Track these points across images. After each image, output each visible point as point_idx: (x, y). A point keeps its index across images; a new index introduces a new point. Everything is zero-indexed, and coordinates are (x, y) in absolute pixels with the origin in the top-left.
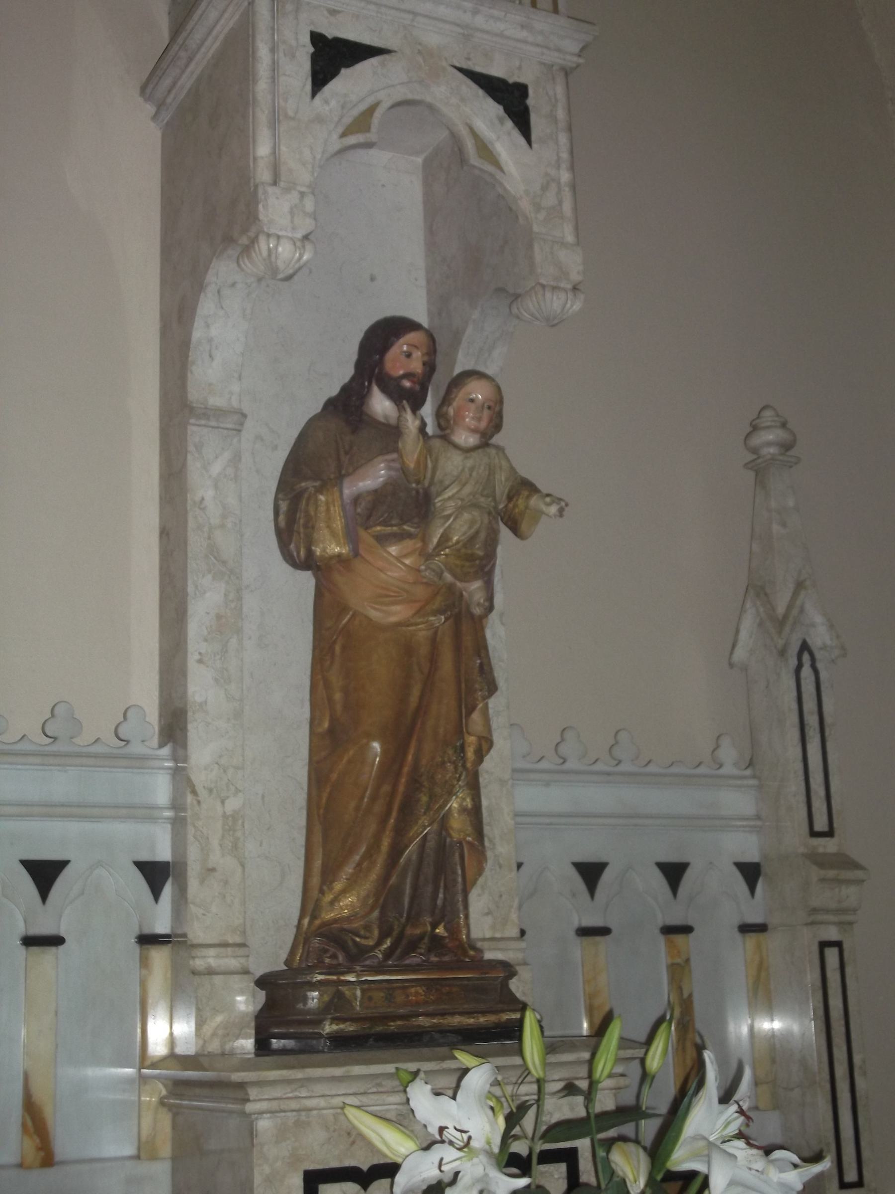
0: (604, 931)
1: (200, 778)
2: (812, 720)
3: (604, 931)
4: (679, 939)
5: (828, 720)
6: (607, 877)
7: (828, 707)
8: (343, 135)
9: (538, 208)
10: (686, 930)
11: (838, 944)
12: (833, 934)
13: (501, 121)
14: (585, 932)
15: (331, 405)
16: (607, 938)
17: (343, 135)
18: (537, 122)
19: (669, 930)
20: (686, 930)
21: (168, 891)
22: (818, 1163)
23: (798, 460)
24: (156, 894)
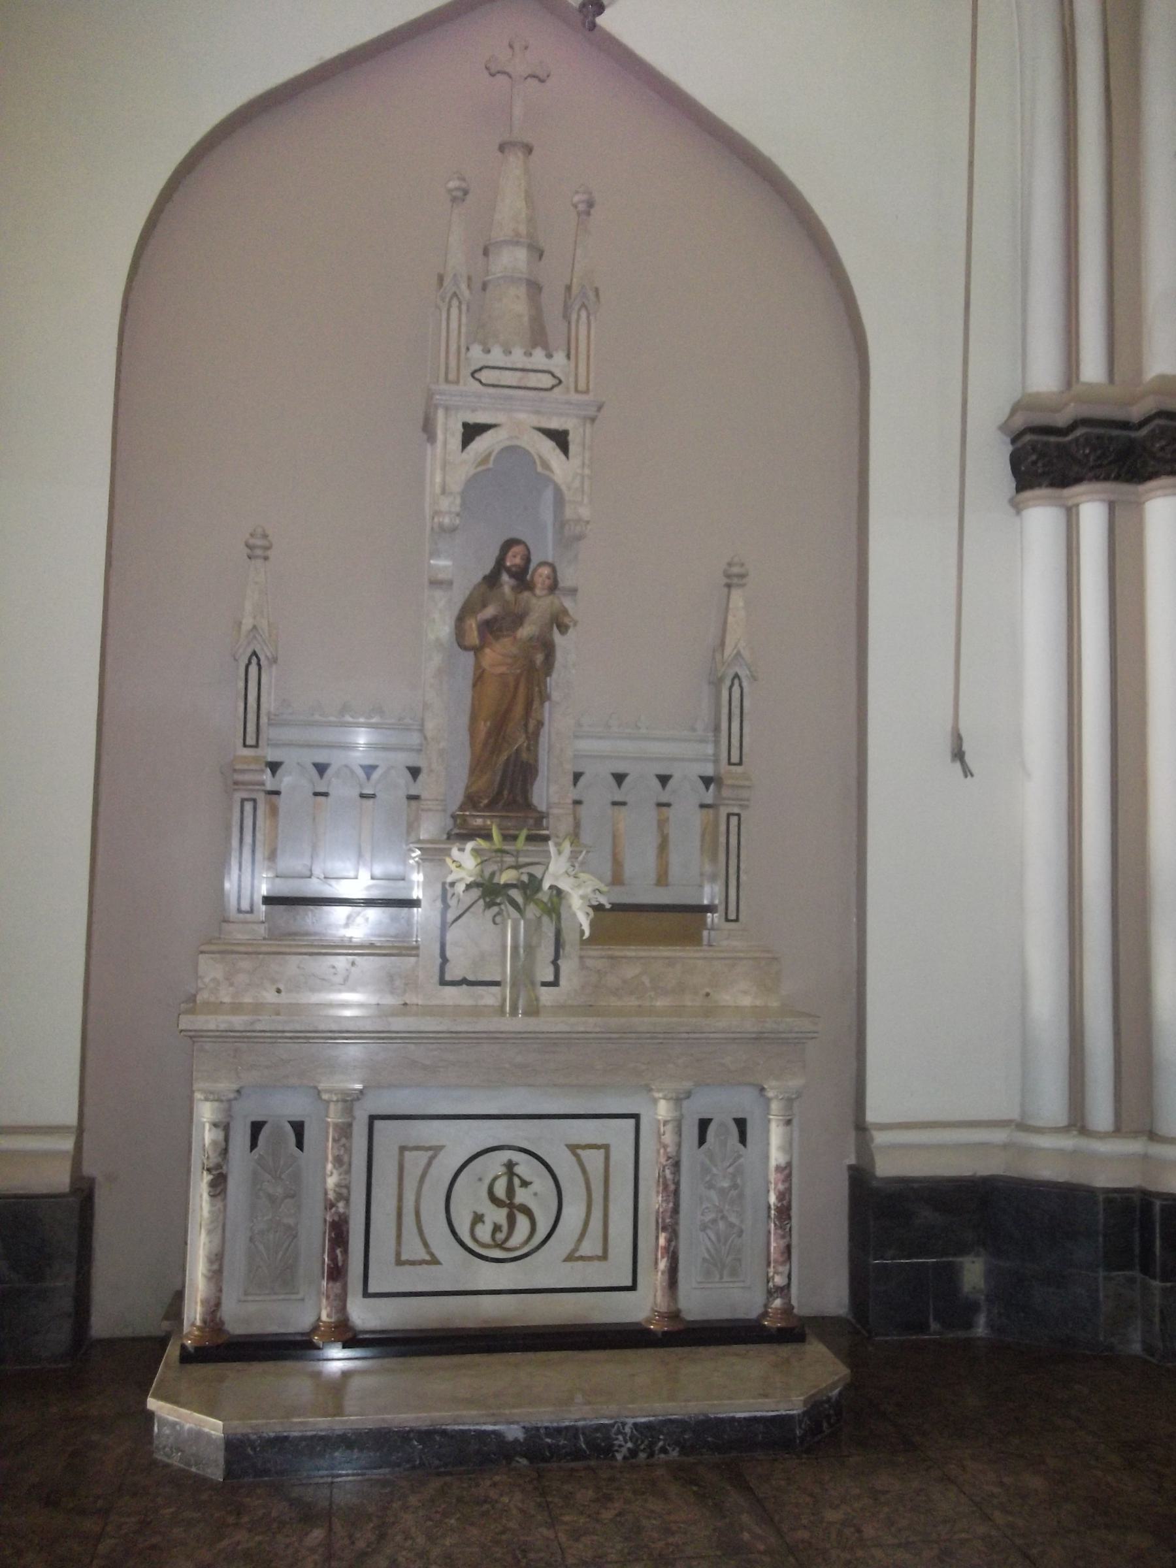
0: (623, 804)
1: (429, 734)
2: (736, 711)
3: (623, 804)
4: (664, 809)
5: (746, 711)
6: (628, 780)
7: (746, 703)
8: (477, 467)
9: (569, 488)
10: (668, 805)
11: (738, 815)
12: (736, 810)
13: (554, 450)
14: (615, 804)
15: (485, 578)
16: (626, 807)
17: (477, 467)
18: (573, 448)
19: (660, 805)
20: (668, 805)
21: (712, 787)
22: (278, 809)
23: (743, 585)
24: (707, 788)
